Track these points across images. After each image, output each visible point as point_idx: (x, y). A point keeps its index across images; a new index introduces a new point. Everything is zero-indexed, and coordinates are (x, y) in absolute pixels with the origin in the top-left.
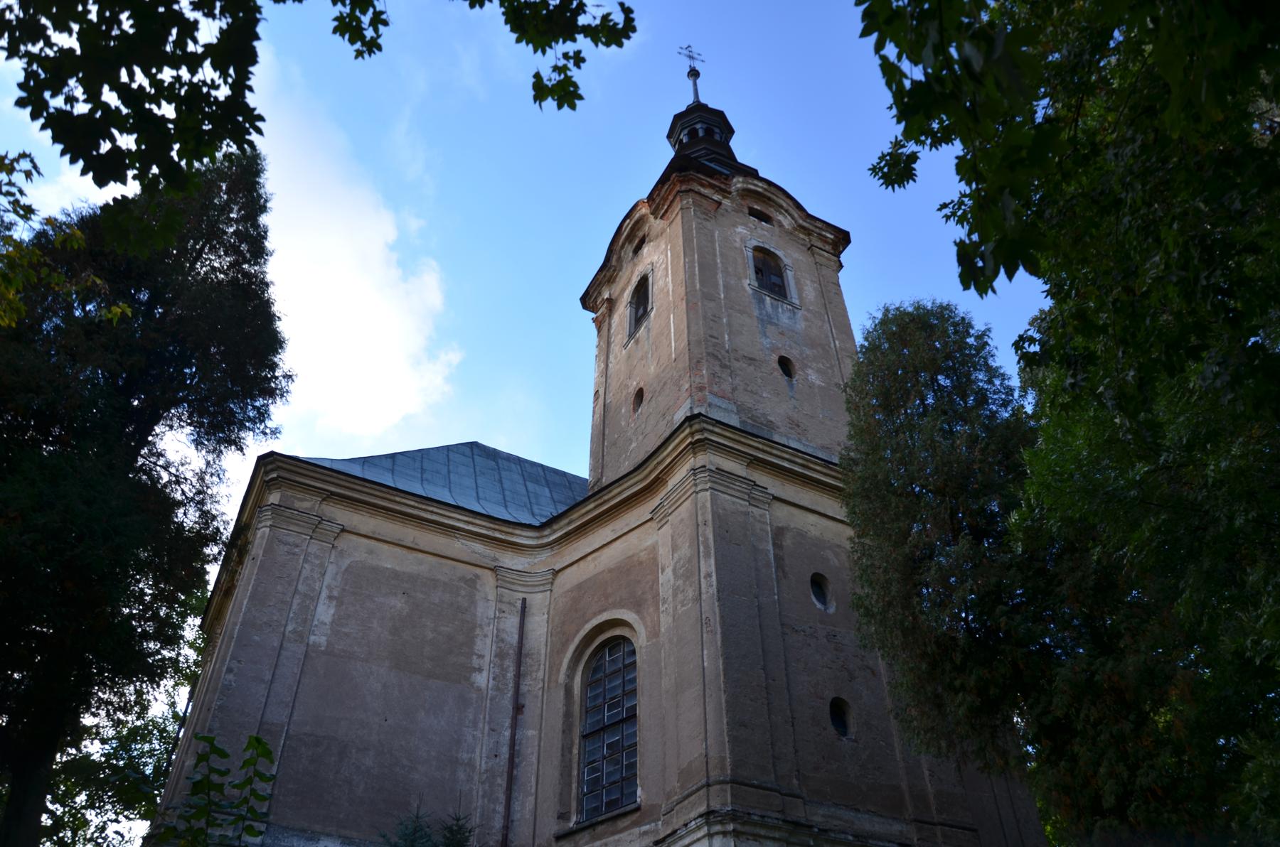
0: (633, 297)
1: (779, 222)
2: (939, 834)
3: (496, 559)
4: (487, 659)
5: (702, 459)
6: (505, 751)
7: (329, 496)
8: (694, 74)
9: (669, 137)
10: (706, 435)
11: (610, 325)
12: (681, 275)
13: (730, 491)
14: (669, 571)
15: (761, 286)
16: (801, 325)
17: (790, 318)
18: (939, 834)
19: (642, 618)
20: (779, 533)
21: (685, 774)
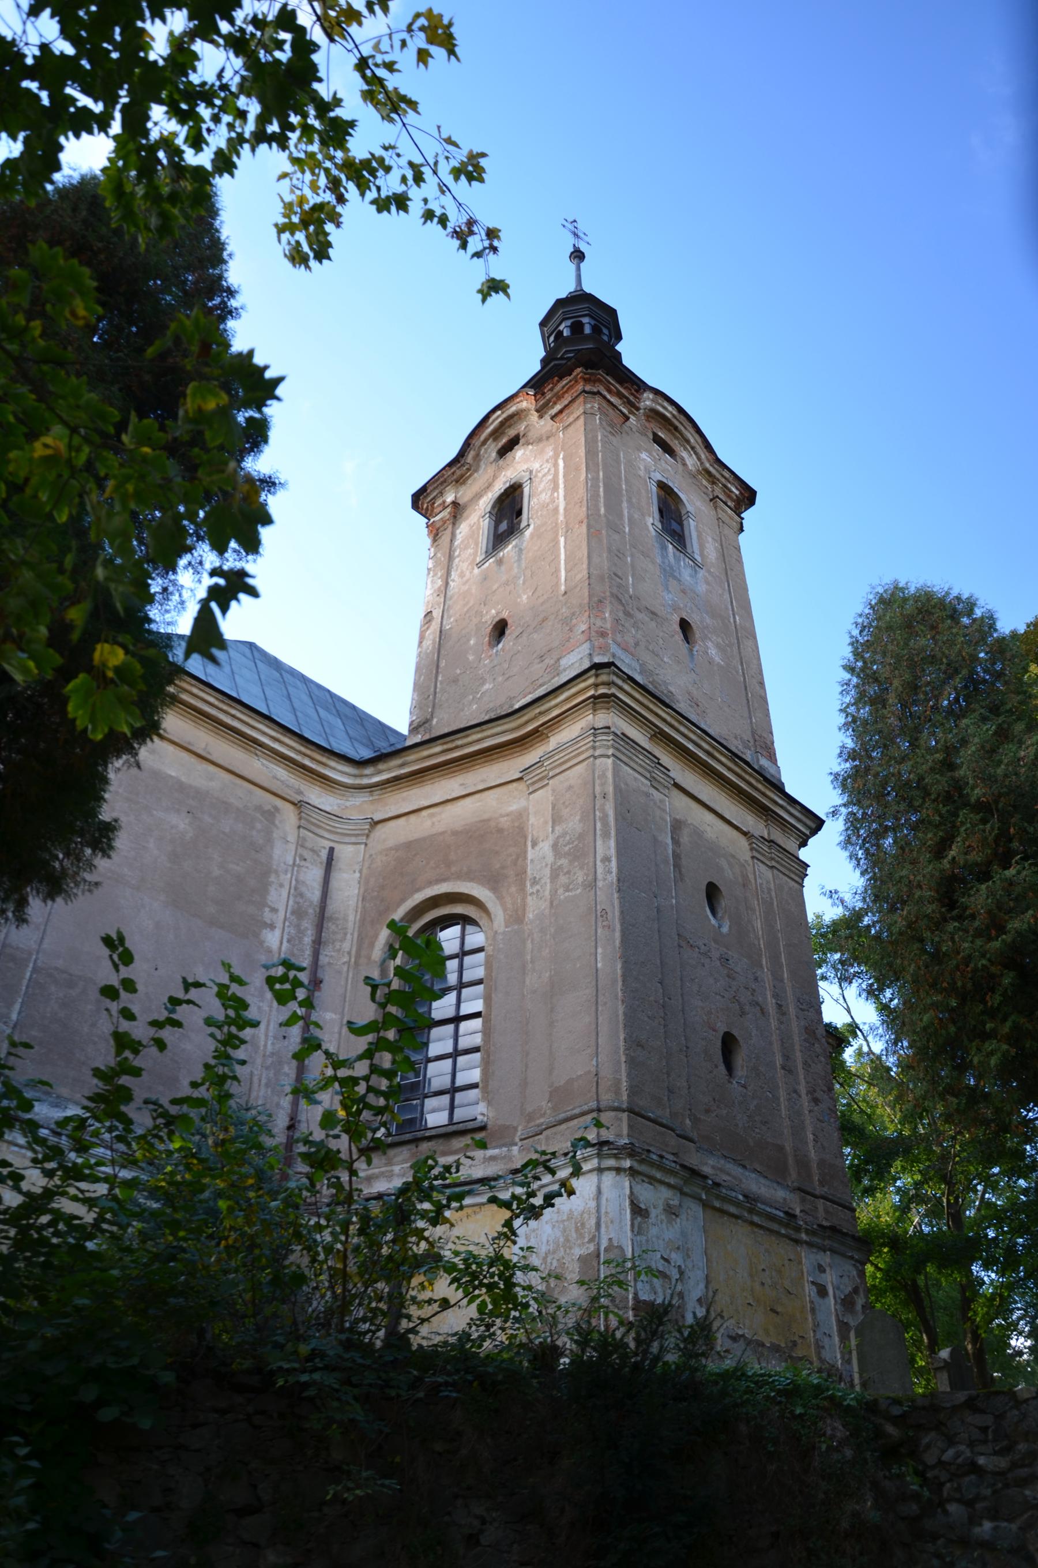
0: (493, 507)
1: (683, 459)
2: (821, 1208)
5: (603, 718)
8: (578, 255)
9: (543, 324)
11: (453, 536)
12: (581, 492)
14: (545, 847)
15: (664, 529)
16: (702, 588)
17: (691, 576)
18: (821, 1208)
19: (500, 898)
20: (677, 826)
21: (559, 1095)
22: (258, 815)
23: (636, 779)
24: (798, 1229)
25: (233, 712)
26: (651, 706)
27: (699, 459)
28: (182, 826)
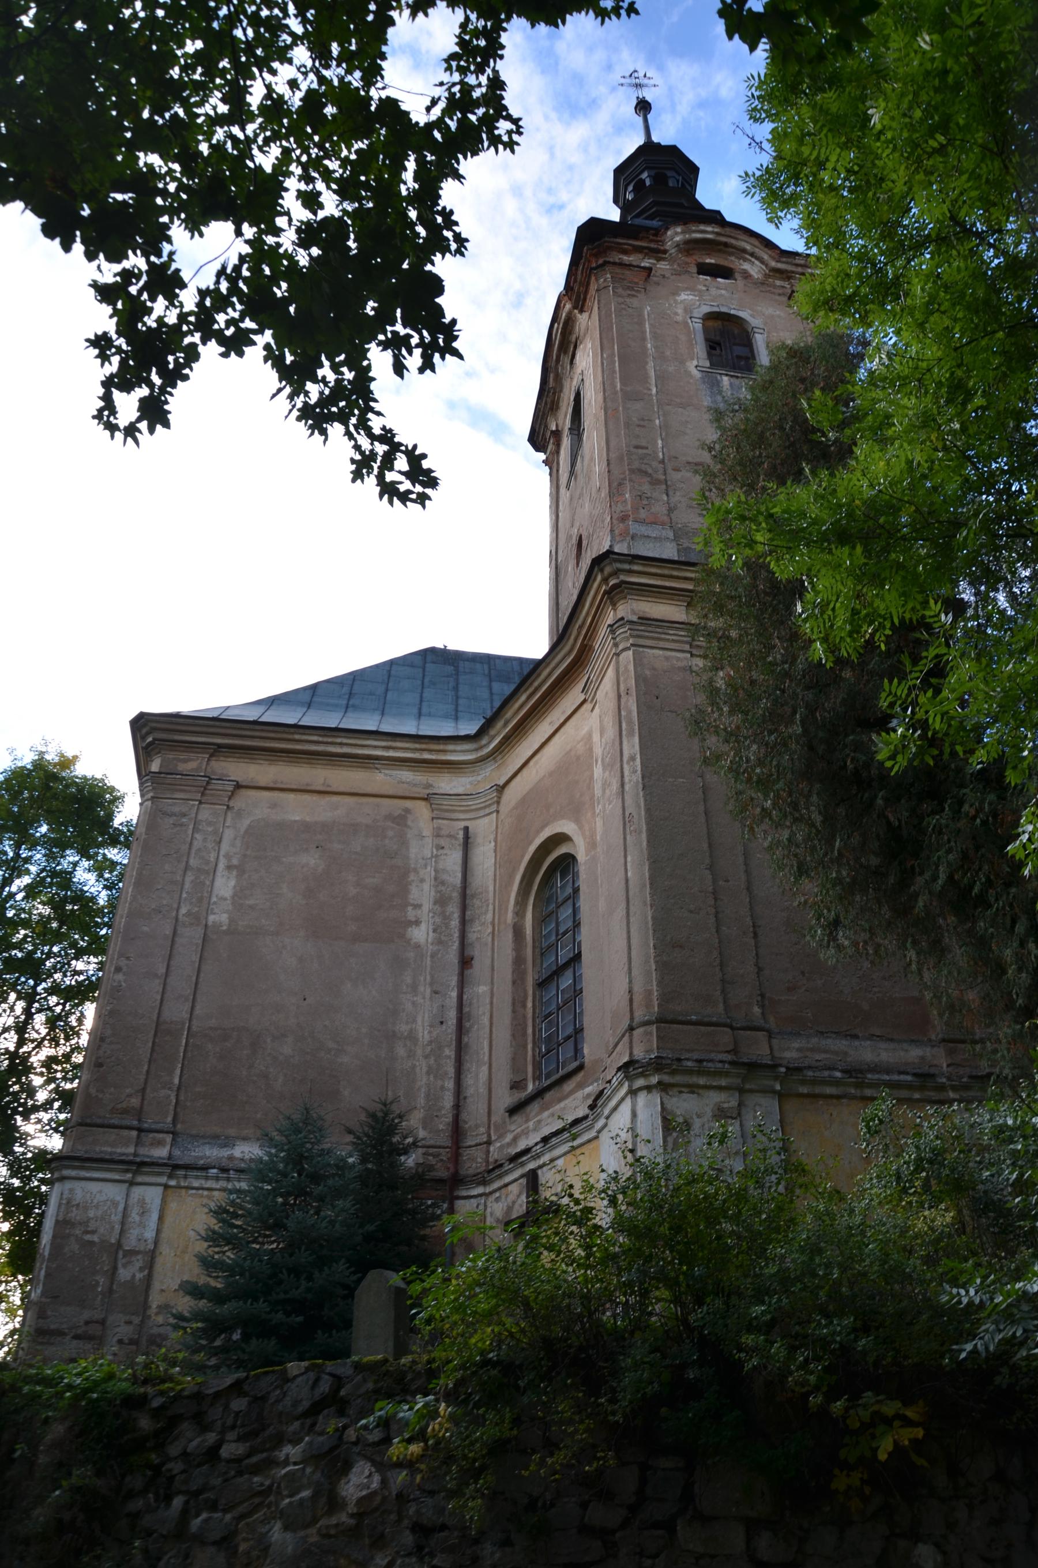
3: (429, 786)
4: (426, 907)
5: (628, 608)
6: (452, 1014)
7: (217, 751)
8: (643, 107)
10: (622, 577)
13: (661, 644)
19: (581, 827)
22: (389, 824)
23: (667, 658)
24: (942, 1088)
25: (339, 740)
26: (675, 573)
27: (762, 262)
28: (312, 862)
